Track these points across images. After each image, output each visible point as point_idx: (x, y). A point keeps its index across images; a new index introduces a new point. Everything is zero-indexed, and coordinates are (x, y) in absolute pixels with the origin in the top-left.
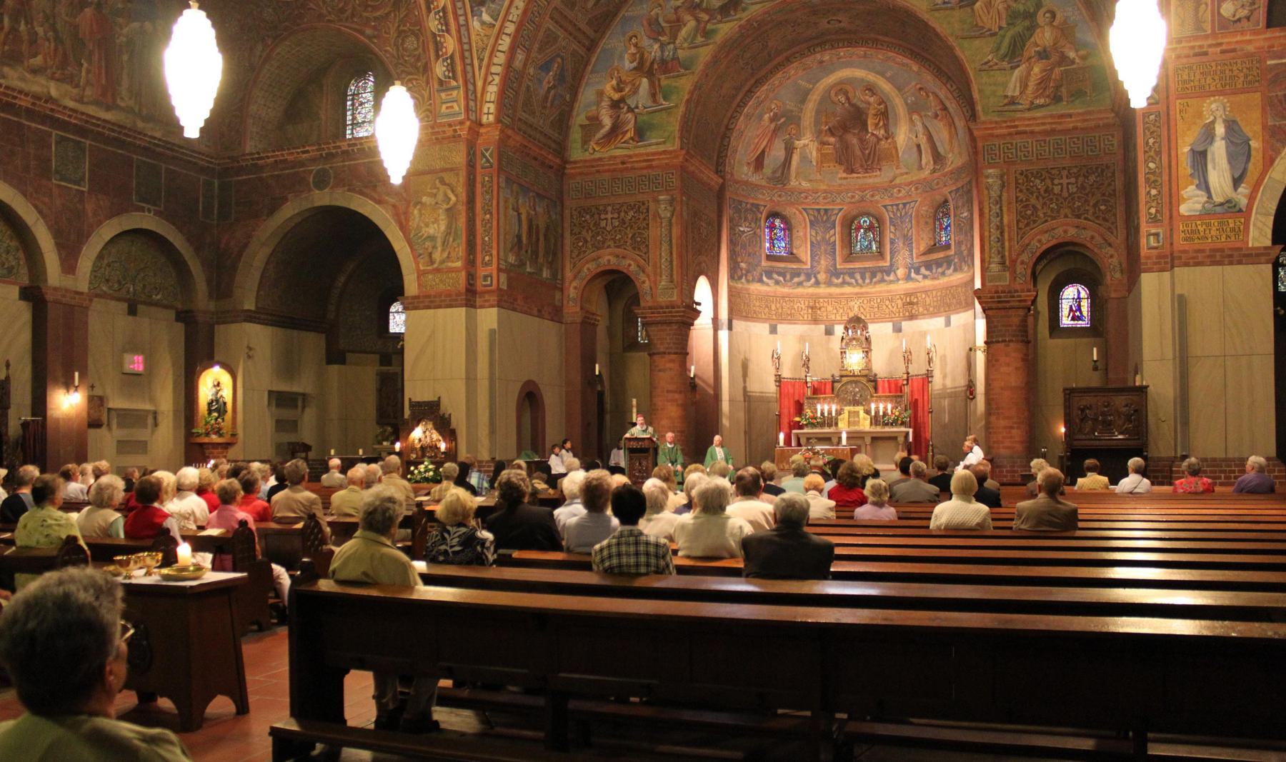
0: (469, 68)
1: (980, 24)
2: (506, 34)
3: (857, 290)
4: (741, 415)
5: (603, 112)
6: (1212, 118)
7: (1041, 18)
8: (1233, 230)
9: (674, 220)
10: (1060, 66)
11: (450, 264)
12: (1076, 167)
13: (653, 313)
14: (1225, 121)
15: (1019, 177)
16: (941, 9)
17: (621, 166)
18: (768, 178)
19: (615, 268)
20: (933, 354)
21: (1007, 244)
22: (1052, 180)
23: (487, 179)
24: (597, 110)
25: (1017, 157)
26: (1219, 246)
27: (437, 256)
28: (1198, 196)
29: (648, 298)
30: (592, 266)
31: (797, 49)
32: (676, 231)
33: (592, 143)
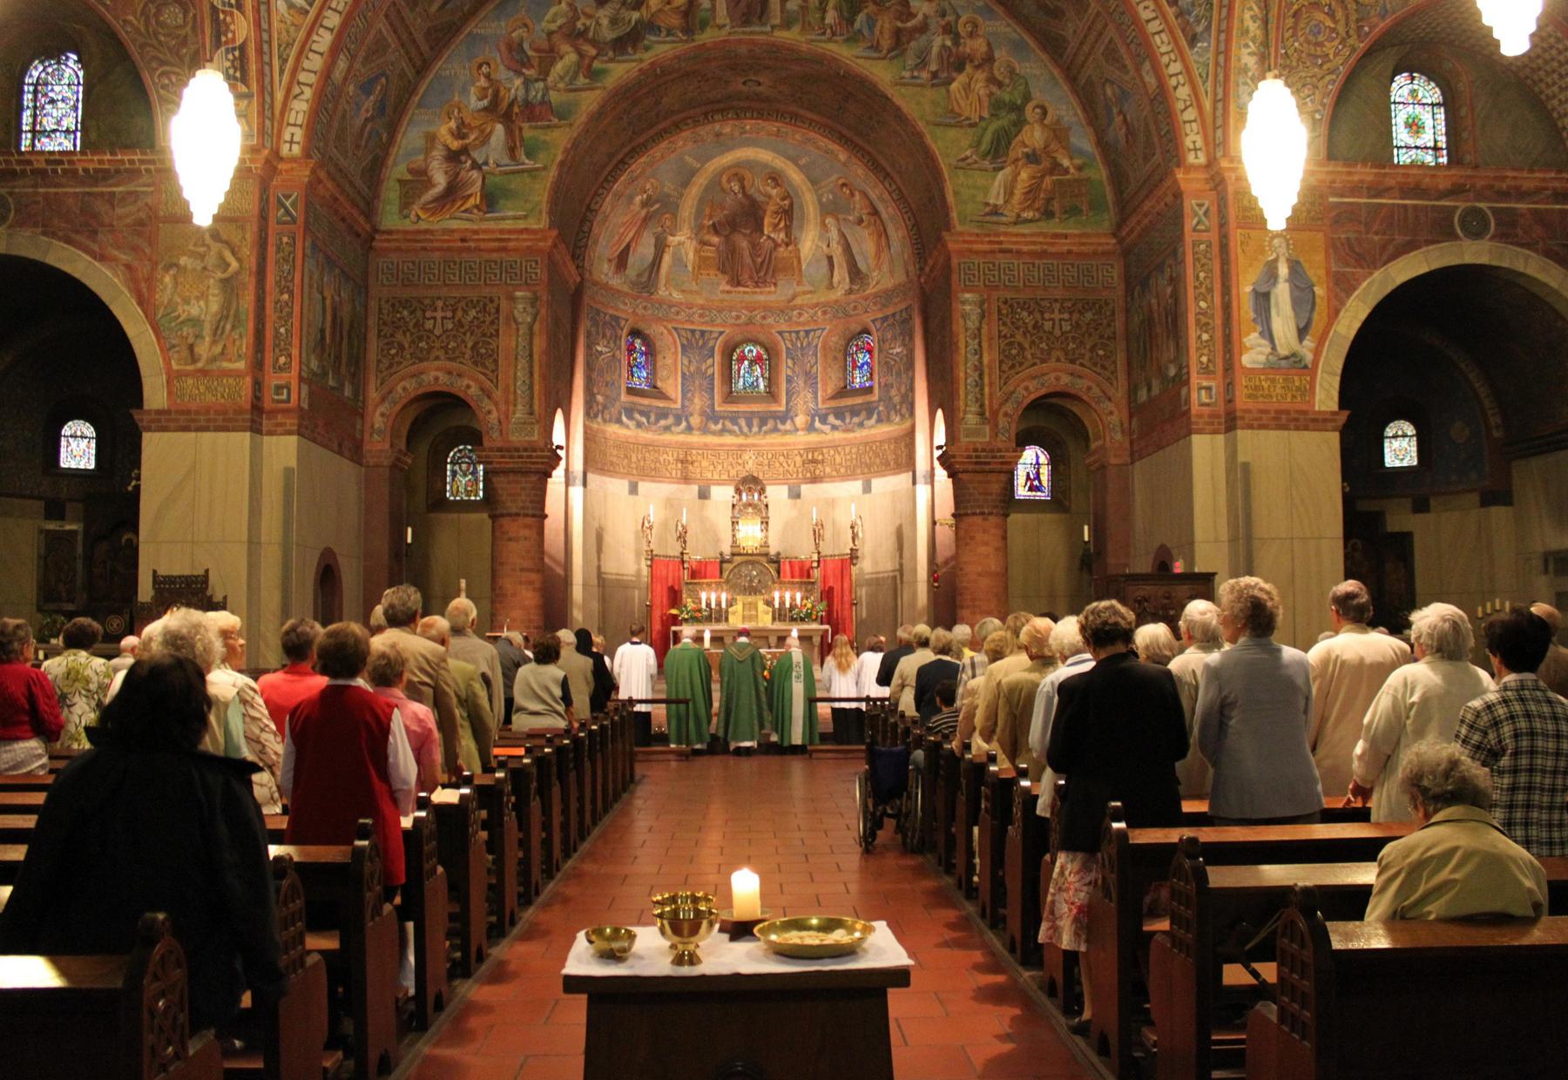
0: (267, 68)
1: (956, 109)
2: (326, 28)
3: (740, 440)
4: (595, 605)
5: (435, 164)
6: (1274, 256)
7: (1031, 113)
8: (1298, 389)
9: (536, 327)
10: (1051, 174)
11: (226, 365)
13: (503, 457)
14: (1288, 260)
15: (1002, 306)
16: (909, 84)
17: (460, 244)
18: (631, 282)
19: (445, 389)
20: (859, 529)
21: (987, 390)
22: (1042, 313)
23: (285, 240)
24: (425, 160)
26: (1284, 407)
27: (203, 349)
28: (1260, 346)
29: (495, 435)
30: (410, 384)
31: (692, 112)
32: (539, 344)
33: (415, 207)
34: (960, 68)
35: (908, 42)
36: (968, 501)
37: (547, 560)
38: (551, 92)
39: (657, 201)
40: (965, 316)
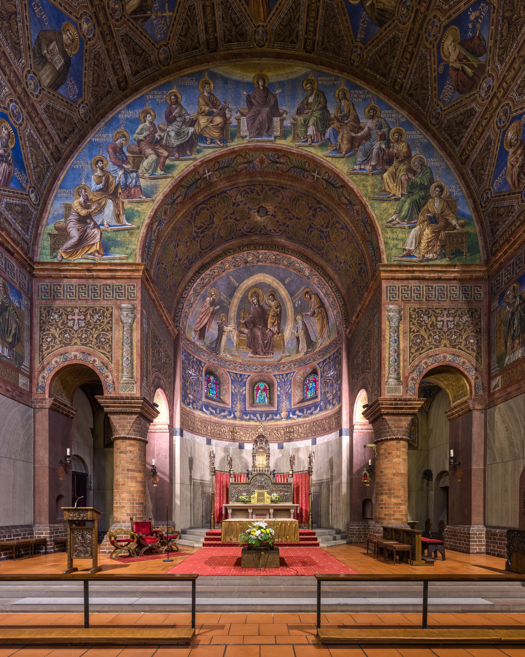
3: (257, 423)
7: (433, 190)
9: (134, 326)
10: (445, 230)
12: (454, 309)
16: (358, 174)
21: (402, 364)
24: (65, 222)
25: (411, 297)
32: (137, 336)
34: (390, 163)
35: (358, 146)
36: (389, 432)
37: (147, 466)
38: (140, 179)
39: (218, 304)
40: (390, 319)
